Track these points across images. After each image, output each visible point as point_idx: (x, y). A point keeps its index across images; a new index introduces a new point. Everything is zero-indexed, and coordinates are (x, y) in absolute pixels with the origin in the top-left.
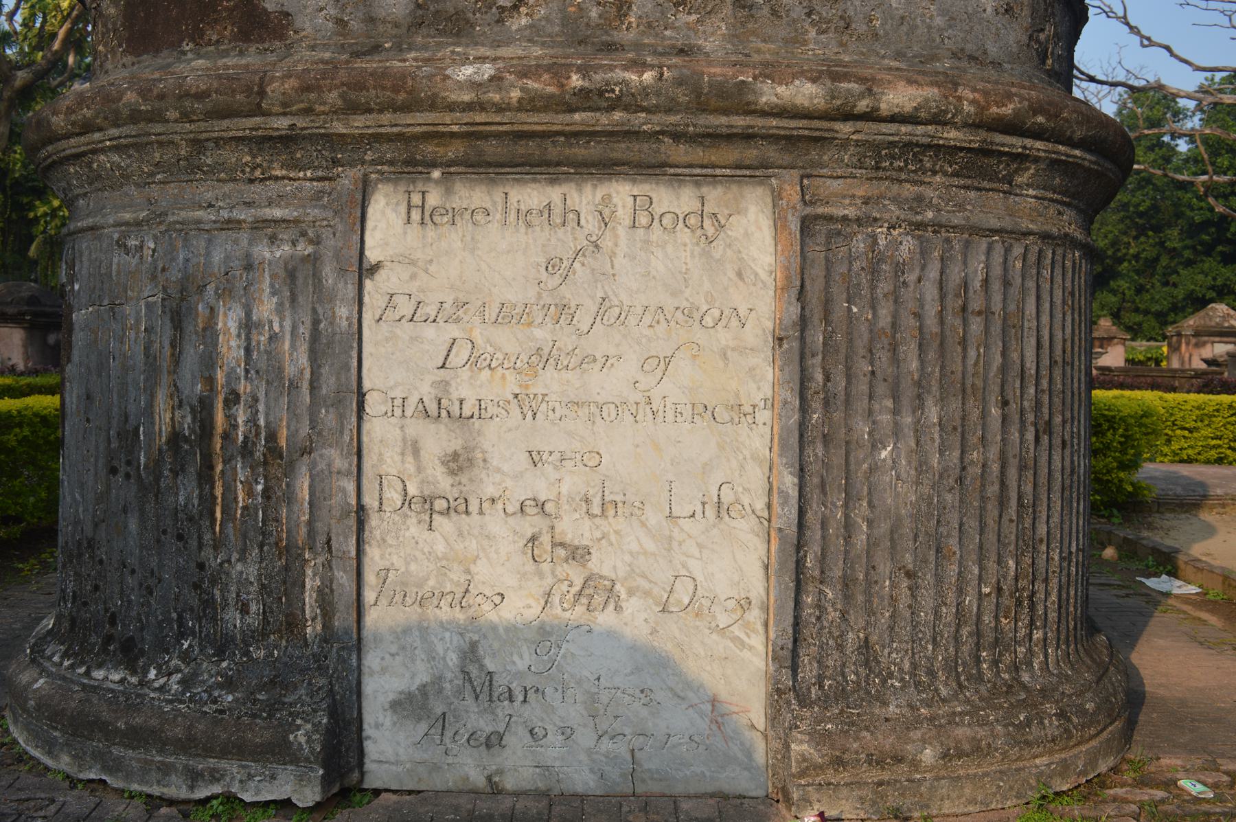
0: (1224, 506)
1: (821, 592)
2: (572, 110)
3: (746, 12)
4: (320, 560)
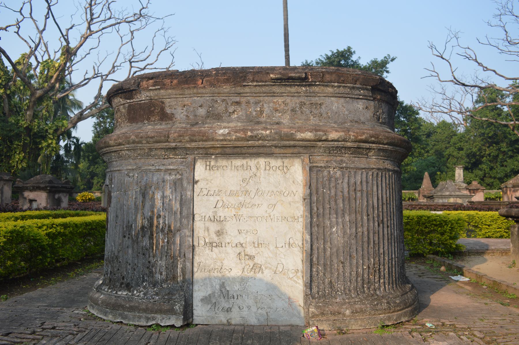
0: (493, 253)
1: (318, 268)
2: (248, 141)
3: (294, 113)
4: (182, 260)
